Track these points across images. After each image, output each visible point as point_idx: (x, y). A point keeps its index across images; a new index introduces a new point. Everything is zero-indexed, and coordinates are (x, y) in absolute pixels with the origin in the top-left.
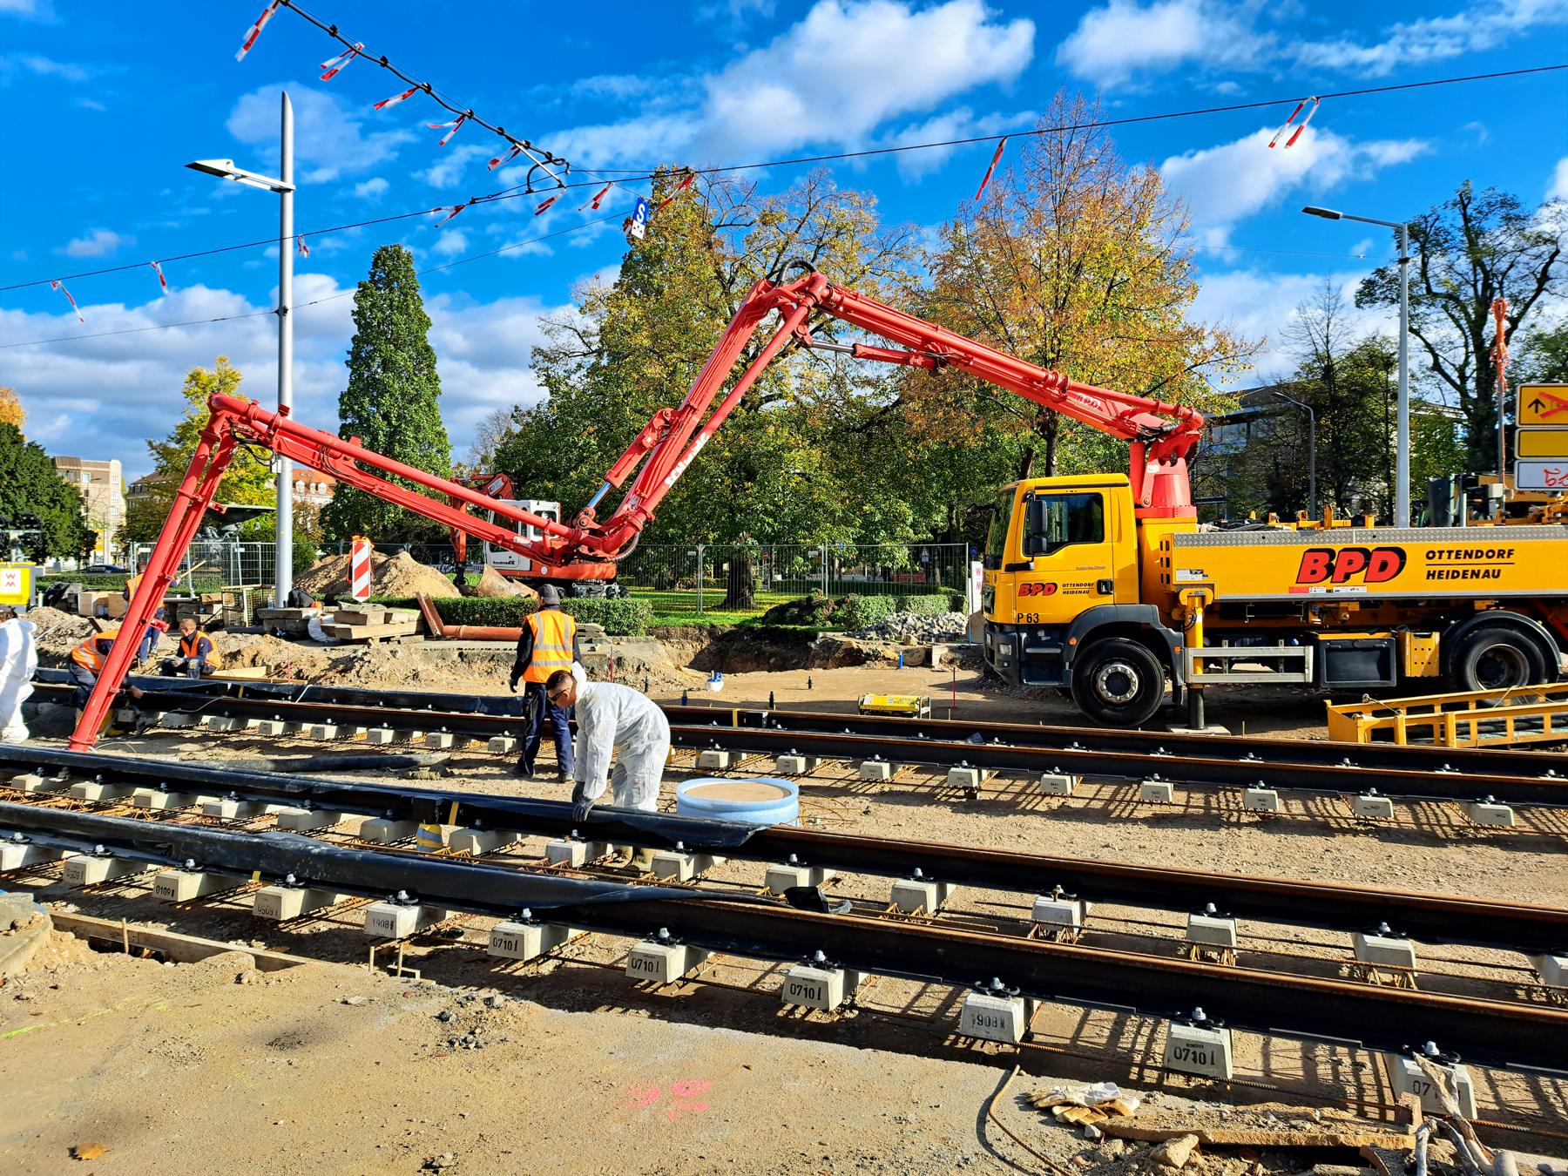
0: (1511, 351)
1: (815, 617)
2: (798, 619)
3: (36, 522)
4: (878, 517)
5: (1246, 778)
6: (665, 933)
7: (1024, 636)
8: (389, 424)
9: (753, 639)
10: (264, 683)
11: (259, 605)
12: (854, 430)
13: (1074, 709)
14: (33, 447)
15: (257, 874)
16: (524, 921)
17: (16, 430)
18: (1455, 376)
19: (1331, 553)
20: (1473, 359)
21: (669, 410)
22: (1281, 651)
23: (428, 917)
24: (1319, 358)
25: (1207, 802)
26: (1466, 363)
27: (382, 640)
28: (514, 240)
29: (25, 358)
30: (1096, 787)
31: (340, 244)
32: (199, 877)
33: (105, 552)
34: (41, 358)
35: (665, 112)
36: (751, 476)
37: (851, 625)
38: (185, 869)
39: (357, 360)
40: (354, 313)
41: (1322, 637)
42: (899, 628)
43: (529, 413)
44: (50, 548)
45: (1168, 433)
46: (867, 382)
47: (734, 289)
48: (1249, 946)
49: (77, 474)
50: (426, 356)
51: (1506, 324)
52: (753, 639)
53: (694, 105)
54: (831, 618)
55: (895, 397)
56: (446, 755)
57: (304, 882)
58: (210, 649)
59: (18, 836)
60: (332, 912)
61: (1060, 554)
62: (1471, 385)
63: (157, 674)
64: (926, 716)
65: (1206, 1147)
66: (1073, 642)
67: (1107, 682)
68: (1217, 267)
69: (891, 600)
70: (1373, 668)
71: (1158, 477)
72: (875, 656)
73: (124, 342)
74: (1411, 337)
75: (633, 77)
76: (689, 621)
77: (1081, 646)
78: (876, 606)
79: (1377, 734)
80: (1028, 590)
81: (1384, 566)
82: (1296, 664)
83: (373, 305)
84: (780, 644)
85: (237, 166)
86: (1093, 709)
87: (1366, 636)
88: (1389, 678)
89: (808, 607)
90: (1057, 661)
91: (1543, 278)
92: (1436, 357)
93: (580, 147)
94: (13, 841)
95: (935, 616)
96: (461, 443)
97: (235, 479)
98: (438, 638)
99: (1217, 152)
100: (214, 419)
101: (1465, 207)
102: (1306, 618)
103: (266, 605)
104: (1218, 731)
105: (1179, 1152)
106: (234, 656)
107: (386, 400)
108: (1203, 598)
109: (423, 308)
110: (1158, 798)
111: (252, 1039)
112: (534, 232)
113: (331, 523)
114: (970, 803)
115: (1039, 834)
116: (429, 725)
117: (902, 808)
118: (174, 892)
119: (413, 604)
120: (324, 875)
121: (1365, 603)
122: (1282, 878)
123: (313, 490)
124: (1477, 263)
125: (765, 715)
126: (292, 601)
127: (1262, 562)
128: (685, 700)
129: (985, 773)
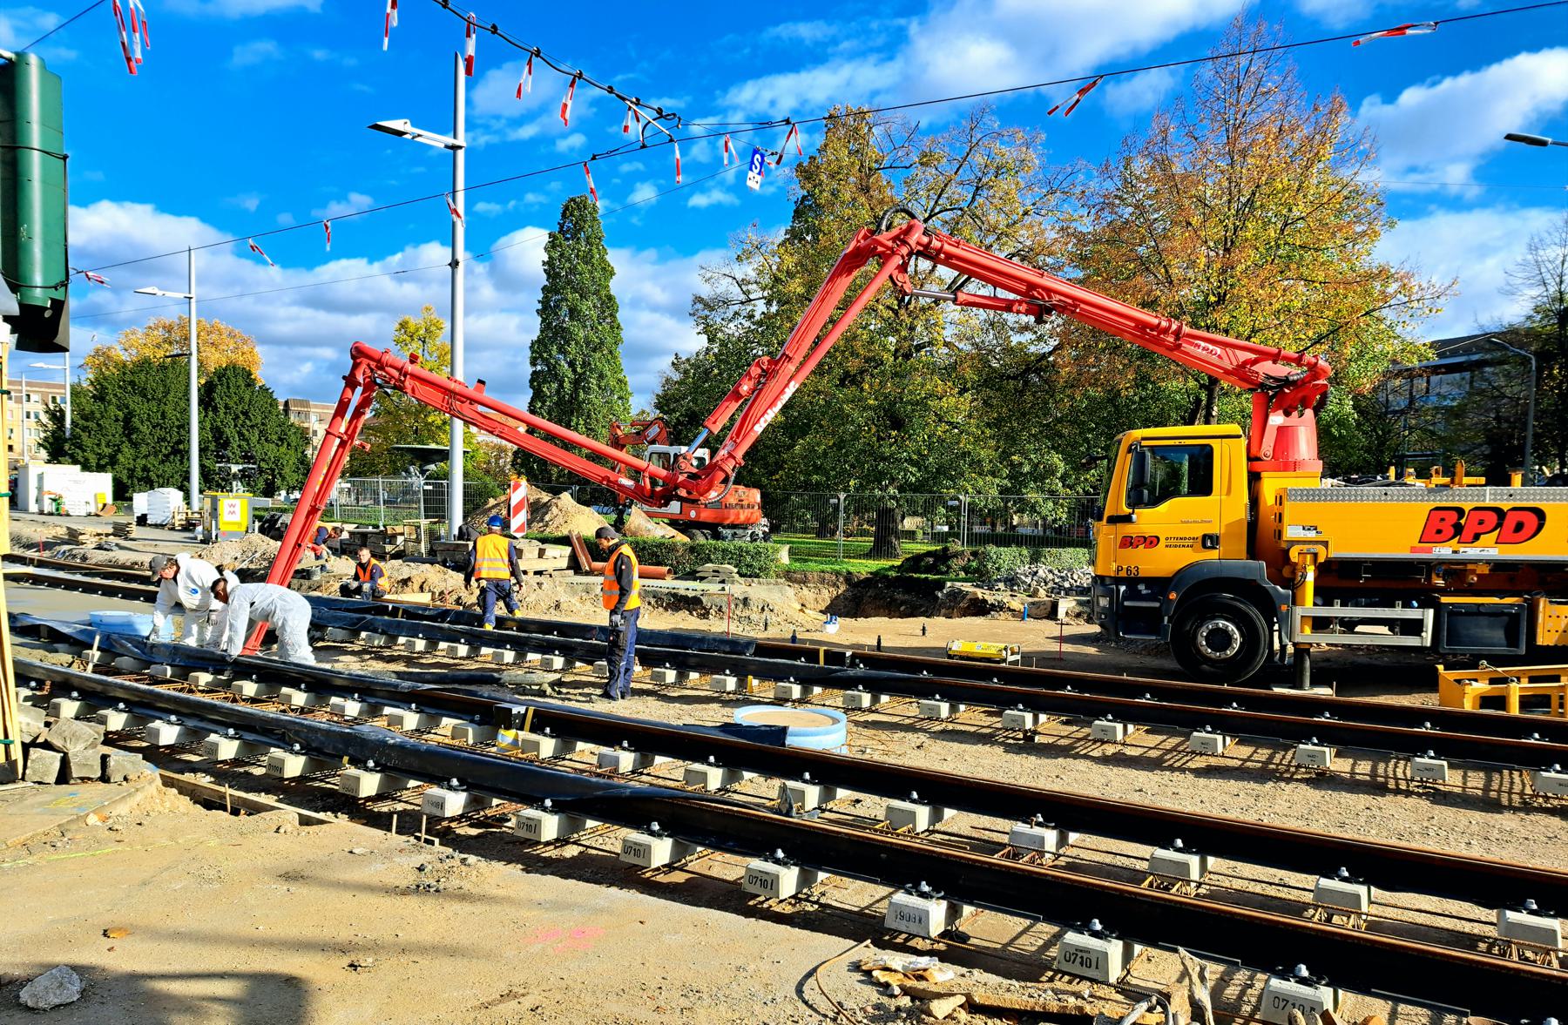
1: (949, 567)
2: (929, 569)
3: (252, 457)
4: (1026, 469)
5: (1416, 746)
6: (656, 827)
7: (1123, 588)
8: (574, 371)
9: (887, 587)
10: (425, 608)
11: (433, 536)
12: (1009, 377)
13: (1171, 664)
14: (264, 389)
15: (346, 759)
16: (545, 809)
17: (250, 374)
19: (1460, 511)
21: (765, 359)
22: (1398, 612)
23: (475, 803)
25: (1374, 769)
27: (536, 573)
28: (704, 191)
29: (283, 312)
30: (1250, 750)
31: (542, 199)
32: (302, 759)
34: (294, 310)
35: (852, 56)
36: (898, 423)
37: (982, 575)
38: (292, 752)
39: (547, 310)
40: (544, 263)
41: (1444, 600)
42: (1028, 580)
44: (278, 482)
45: (1294, 382)
48: (1227, 884)
49: (307, 415)
50: (608, 305)
52: (887, 587)
53: (893, 46)
54: (966, 569)
55: (1053, 343)
56: (558, 676)
57: (381, 767)
58: (382, 575)
59: (173, 718)
60: (405, 795)
61: (1164, 507)
63: (337, 596)
64: (1016, 663)
65: (972, 1007)
66: (1173, 596)
67: (1207, 638)
68: (1456, 204)
69: (1025, 552)
70: (1499, 635)
71: (1281, 429)
72: (1000, 607)
73: (366, 297)
75: (821, 23)
76: (828, 567)
77: (1180, 601)
78: (1007, 557)
79: (1486, 701)
80: (1128, 542)
81: (1519, 527)
82: (1415, 627)
83: (562, 255)
84: (912, 591)
86: (1192, 664)
87: (1495, 600)
88: (1517, 646)
89: (943, 557)
90: (1156, 614)
93: (767, 95)
94: (169, 722)
95: (1070, 570)
96: (641, 391)
97: (439, 422)
98: (587, 574)
99: (1465, 80)
100: (355, 366)
102: (1429, 578)
103: (439, 538)
104: (1325, 692)
105: (940, 1008)
106: (405, 582)
107: (572, 348)
108: (1315, 555)
109: (608, 258)
110: (1206, 749)
111: (266, 871)
112: (722, 183)
113: (522, 465)
114: (1028, 745)
115: (1078, 776)
116: (546, 648)
117: (955, 745)
118: (281, 770)
119: (565, 541)
120: (403, 764)
121: (1499, 566)
122: (1305, 829)
125: (848, 654)
126: (462, 535)
127: (1385, 521)
128: (794, 639)
129: (1131, 728)
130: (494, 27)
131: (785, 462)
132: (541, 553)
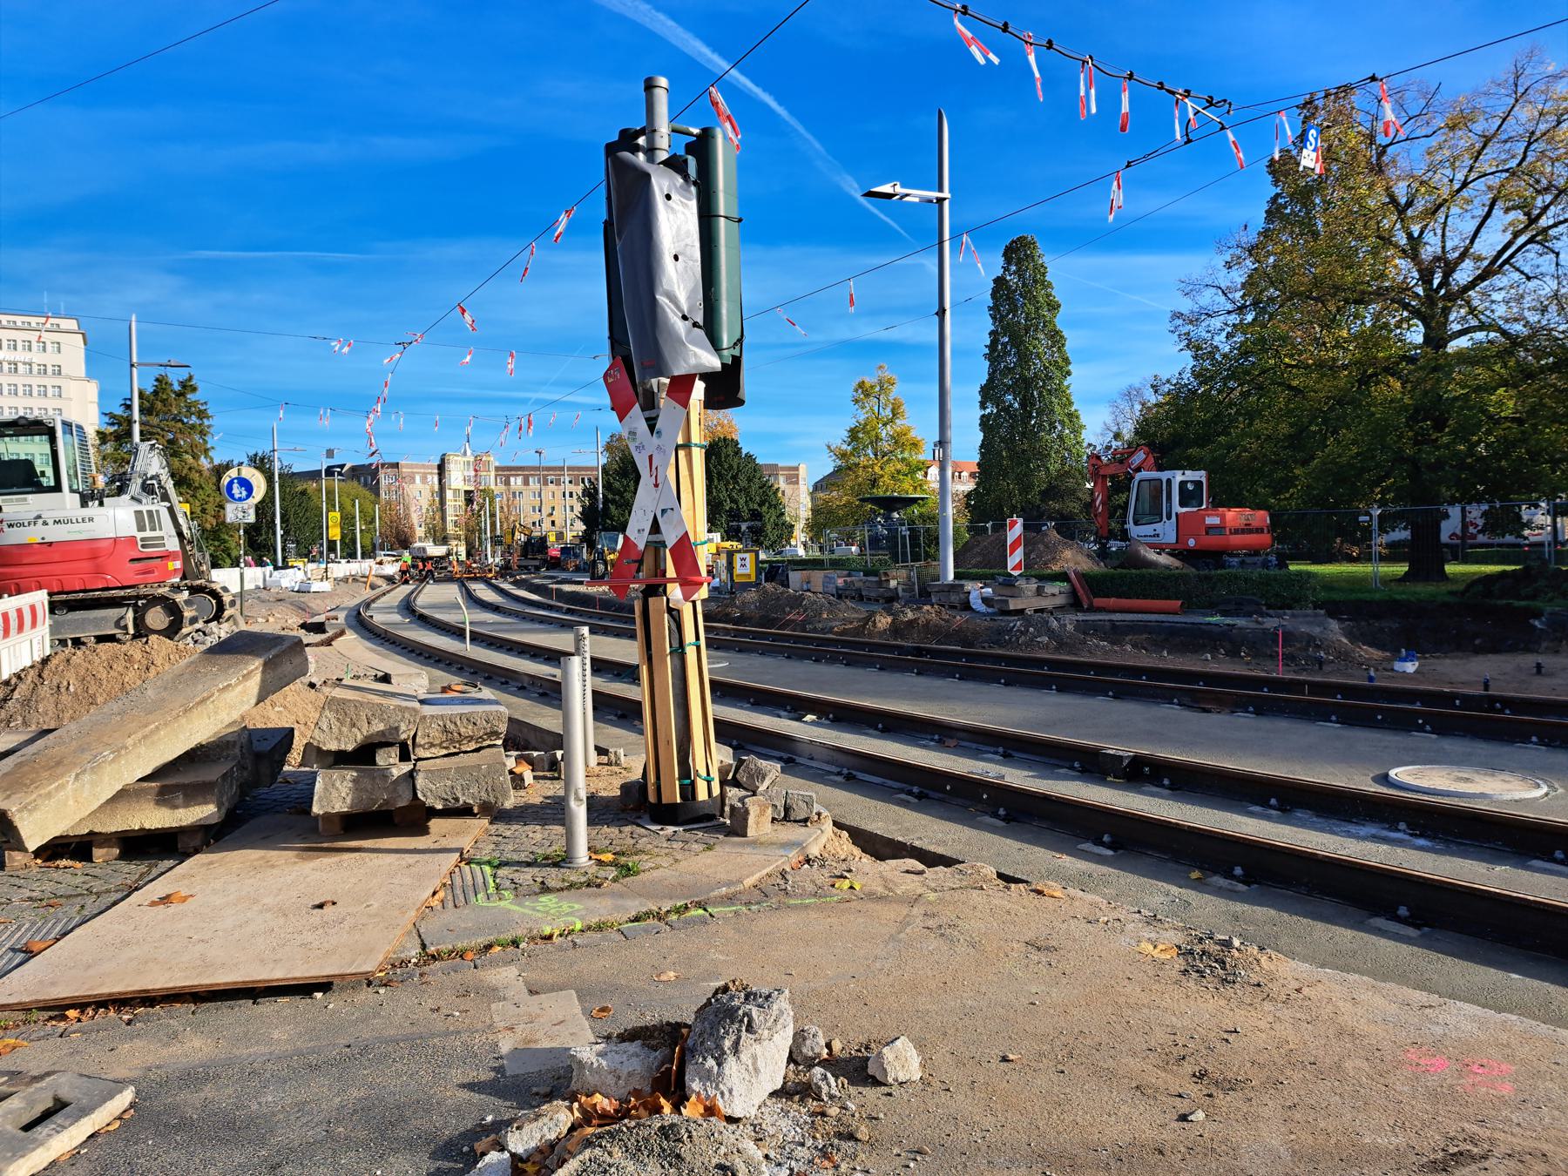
14: (749, 456)
33: (799, 545)
43: (1168, 381)
47: (1409, 212)
49: (776, 479)
50: (1056, 338)
131: (1296, 478)
132: (1039, 592)
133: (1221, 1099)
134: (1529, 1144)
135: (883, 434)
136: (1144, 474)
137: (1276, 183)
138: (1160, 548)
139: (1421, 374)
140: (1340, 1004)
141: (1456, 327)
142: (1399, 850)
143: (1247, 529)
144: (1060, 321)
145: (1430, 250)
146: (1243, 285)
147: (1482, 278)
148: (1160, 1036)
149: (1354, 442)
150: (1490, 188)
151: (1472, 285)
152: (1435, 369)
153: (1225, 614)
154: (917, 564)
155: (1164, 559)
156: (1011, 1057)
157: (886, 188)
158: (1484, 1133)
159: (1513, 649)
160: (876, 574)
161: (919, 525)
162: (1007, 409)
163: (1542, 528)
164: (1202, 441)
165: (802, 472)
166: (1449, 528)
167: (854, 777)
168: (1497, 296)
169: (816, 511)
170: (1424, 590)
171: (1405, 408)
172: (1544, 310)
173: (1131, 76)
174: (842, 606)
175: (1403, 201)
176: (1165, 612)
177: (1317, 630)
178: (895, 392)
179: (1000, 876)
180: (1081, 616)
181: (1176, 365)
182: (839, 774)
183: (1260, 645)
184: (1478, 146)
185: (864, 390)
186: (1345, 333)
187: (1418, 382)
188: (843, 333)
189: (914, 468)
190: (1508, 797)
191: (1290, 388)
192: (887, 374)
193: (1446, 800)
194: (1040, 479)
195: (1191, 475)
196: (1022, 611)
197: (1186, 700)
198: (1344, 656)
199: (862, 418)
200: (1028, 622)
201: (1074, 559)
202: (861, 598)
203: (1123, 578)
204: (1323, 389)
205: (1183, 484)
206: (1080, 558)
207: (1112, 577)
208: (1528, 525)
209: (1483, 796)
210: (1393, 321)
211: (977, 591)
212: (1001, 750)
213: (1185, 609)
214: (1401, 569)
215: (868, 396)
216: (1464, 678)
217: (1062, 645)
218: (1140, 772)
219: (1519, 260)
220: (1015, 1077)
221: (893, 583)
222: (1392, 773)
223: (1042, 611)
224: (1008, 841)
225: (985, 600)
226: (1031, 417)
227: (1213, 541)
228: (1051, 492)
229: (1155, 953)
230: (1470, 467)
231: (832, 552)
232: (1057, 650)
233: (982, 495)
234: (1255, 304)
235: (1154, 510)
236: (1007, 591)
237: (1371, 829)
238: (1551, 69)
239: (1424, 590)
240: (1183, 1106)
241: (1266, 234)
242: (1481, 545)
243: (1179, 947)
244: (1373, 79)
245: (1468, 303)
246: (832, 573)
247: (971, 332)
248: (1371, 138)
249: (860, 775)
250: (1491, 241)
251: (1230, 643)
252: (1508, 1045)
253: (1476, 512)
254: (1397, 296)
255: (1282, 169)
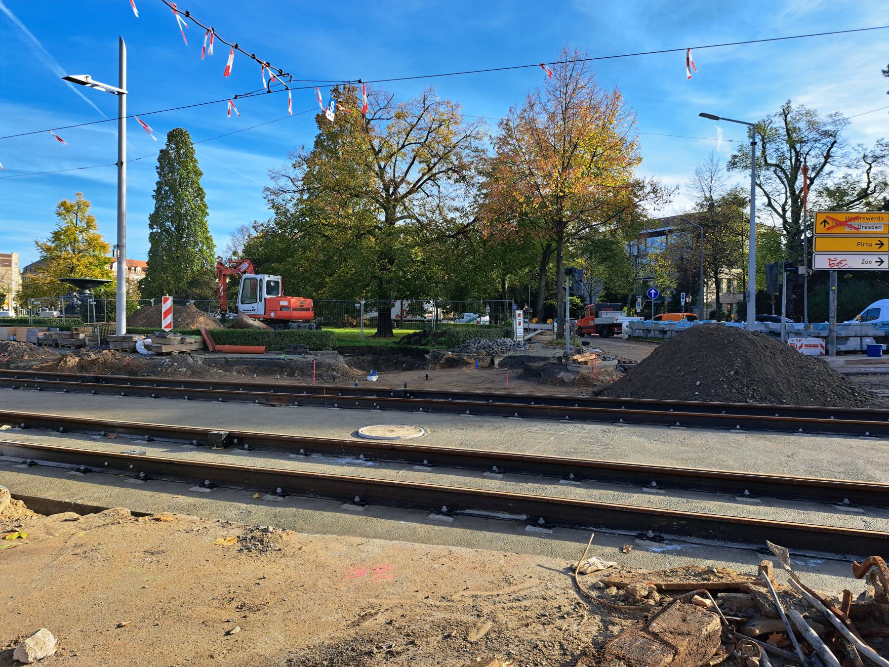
0: (812, 197)
2: (418, 342)
18: (780, 210)
20: (789, 201)
24: (706, 199)
26: (786, 202)
46: (457, 209)
47: (380, 155)
50: (199, 192)
51: (808, 182)
55: (472, 218)
62: (789, 214)
74: (757, 188)
85: (93, 79)
91: (828, 156)
92: (769, 198)
101: (786, 116)
123: (133, 271)
124: (792, 147)
130: (187, 13)
132: (182, 341)
133: (251, 617)
134: (396, 602)
135: (80, 238)
136: (247, 275)
137: (320, 128)
138: (255, 317)
139: (384, 236)
140: (320, 552)
141: (399, 215)
142: (359, 469)
143: (301, 309)
144: (202, 182)
145: (388, 176)
146: (303, 179)
147: (409, 193)
148: (222, 589)
149: (354, 267)
150: (413, 150)
151: (405, 196)
152: (389, 234)
153: (288, 353)
154: (100, 323)
155: (257, 323)
156: (124, 623)
157: (81, 78)
158: (377, 601)
159: (418, 368)
160: (68, 329)
161: (104, 299)
162: (167, 231)
163: (431, 312)
164: (280, 260)
165: (15, 258)
166: (395, 312)
167: (36, 464)
168: (415, 203)
169: (25, 286)
170: (383, 341)
171: (376, 252)
172: (434, 212)
173: (236, 47)
174: (41, 350)
175: (377, 149)
176: (256, 353)
177: (332, 361)
178: (89, 212)
179: (133, 513)
180: (207, 356)
181: (267, 216)
182: (24, 463)
183: (304, 370)
184: (409, 129)
185: (65, 209)
186: (350, 211)
187: (383, 239)
188: (52, 168)
189: (102, 263)
190: (408, 437)
191: (324, 236)
192: (83, 199)
193: (379, 441)
194: (188, 275)
195: (273, 278)
196: (170, 353)
197: (263, 400)
198: (345, 374)
199: (64, 226)
200: (174, 359)
201: (205, 322)
202: (57, 346)
203: (234, 334)
204: (340, 238)
205: (268, 282)
206: (209, 322)
207: (227, 334)
208: (426, 311)
209: (398, 438)
210: (372, 208)
211: (140, 341)
212: (146, 437)
213: (268, 350)
214: (374, 331)
215: (68, 211)
216: (398, 383)
217: (194, 373)
218: (232, 442)
219: (424, 186)
220: (125, 635)
221: (82, 336)
222: (360, 431)
223: (183, 353)
224: (144, 492)
225: (147, 347)
226: (182, 237)
227: (284, 315)
228: (193, 283)
229: (225, 543)
230: (403, 283)
231: (38, 315)
232: (191, 375)
233: (150, 282)
234: (309, 189)
235: (253, 296)
236: (162, 341)
237: (348, 460)
238: (438, 100)
239: (383, 341)
240: (227, 627)
241: (314, 153)
242: (408, 321)
243: (239, 537)
244: (360, 82)
245: (404, 204)
246: (34, 329)
247: (143, 182)
248: (364, 116)
249: (40, 462)
250: (413, 176)
251: (290, 369)
252: (393, 556)
253: (406, 303)
254: (374, 196)
255: (321, 119)
